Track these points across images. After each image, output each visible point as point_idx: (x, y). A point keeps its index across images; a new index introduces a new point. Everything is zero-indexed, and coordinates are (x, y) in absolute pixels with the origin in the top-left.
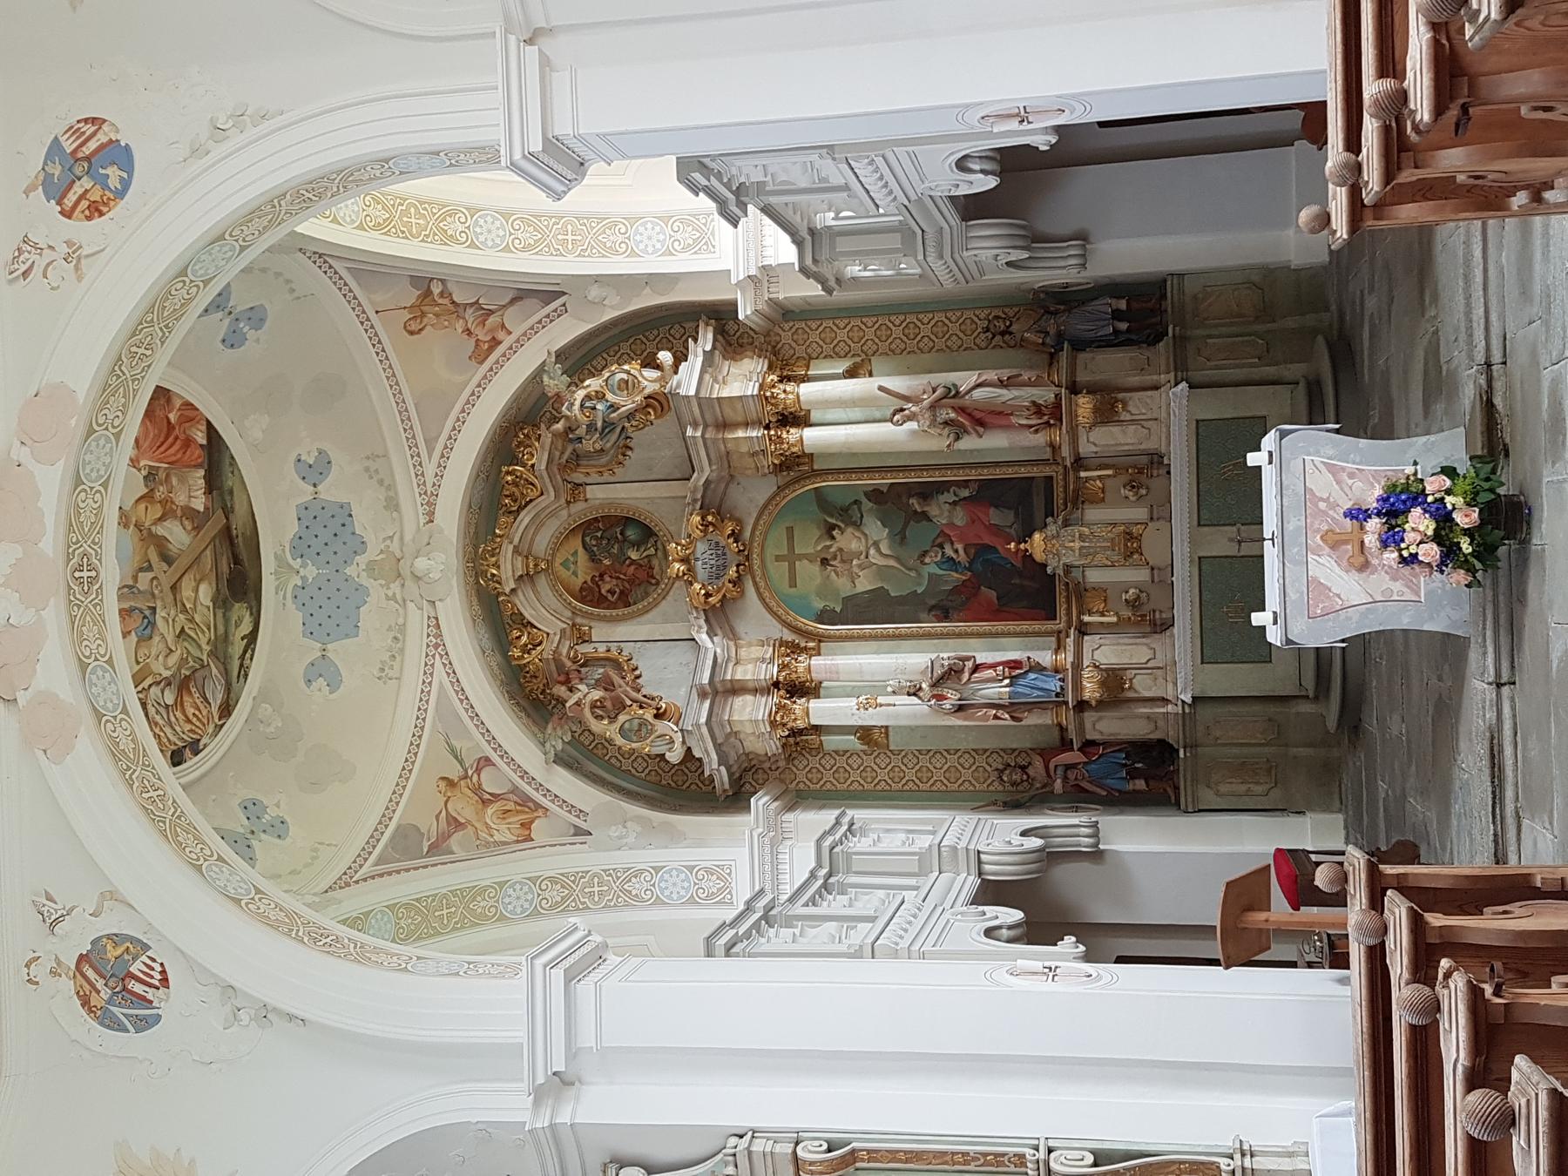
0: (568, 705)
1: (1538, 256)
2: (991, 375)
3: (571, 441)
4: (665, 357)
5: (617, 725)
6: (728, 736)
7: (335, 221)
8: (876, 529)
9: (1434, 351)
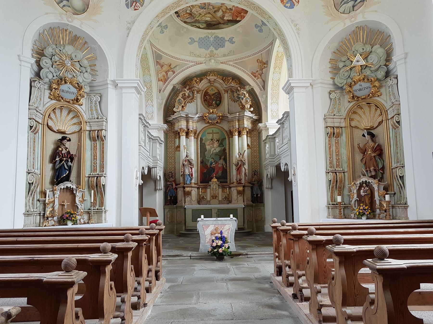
0: (185, 89)
1: (266, 262)
2: (247, 171)
3: (236, 91)
4: (252, 109)
5: (181, 98)
6: (178, 120)
7: (279, 47)
8: (218, 150)
9: (249, 247)
